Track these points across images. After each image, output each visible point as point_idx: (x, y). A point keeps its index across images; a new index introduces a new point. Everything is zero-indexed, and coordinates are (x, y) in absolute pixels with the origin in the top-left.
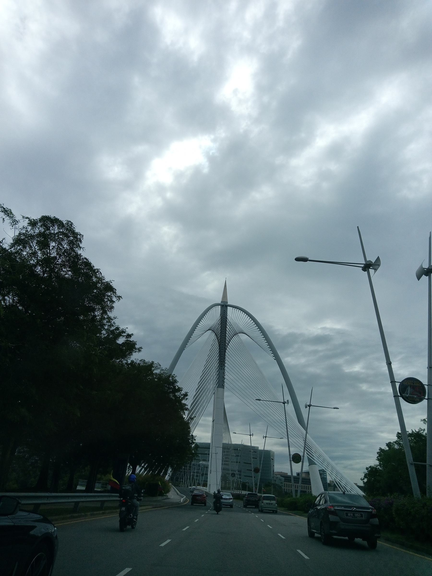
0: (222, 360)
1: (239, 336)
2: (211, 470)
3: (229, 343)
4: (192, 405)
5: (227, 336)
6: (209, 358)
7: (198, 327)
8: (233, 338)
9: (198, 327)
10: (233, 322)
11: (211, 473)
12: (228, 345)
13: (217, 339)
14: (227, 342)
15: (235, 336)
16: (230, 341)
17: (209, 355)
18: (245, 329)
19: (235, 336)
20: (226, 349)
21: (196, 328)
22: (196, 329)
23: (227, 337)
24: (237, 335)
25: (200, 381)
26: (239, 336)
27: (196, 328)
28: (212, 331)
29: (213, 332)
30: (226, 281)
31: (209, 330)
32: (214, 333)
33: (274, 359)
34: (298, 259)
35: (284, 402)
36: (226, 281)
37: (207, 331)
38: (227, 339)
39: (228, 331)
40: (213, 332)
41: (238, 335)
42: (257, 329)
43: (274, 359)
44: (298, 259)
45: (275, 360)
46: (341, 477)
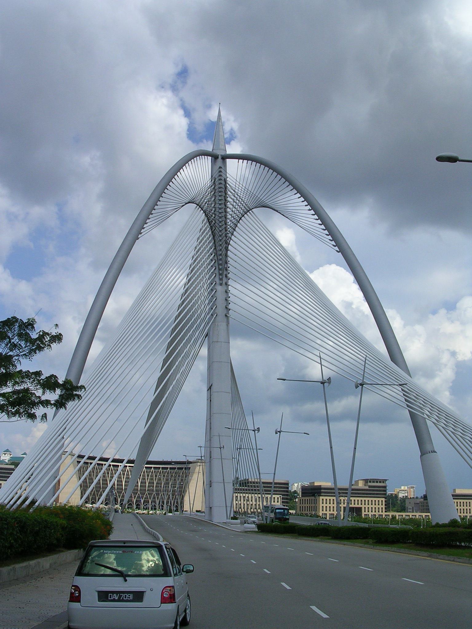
0: (221, 267)
1: (254, 214)
2: (211, 481)
3: (234, 230)
4: (174, 332)
5: (230, 217)
6: (200, 243)
7: (162, 197)
8: (244, 217)
9: (162, 197)
10: (240, 187)
11: (211, 487)
12: (232, 234)
13: (206, 220)
14: (230, 229)
15: (247, 215)
16: (237, 226)
17: (203, 230)
18: (267, 199)
19: (247, 215)
20: (229, 244)
21: (155, 208)
22: (151, 215)
23: (229, 227)
24: (250, 213)
25: (185, 294)
26: (254, 214)
27: (155, 208)
28: (196, 205)
29: (199, 209)
30: (53, 419)
31: (189, 203)
32: (201, 211)
33: (337, 251)
34: (440, 159)
35: (363, 384)
36: (53, 419)
37: (186, 204)
38: (229, 223)
39: (231, 207)
40: (199, 209)
41: (252, 211)
42: (299, 198)
43: (337, 251)
44: (440, 159)
45: (339, 252)
46: (463, 427)
